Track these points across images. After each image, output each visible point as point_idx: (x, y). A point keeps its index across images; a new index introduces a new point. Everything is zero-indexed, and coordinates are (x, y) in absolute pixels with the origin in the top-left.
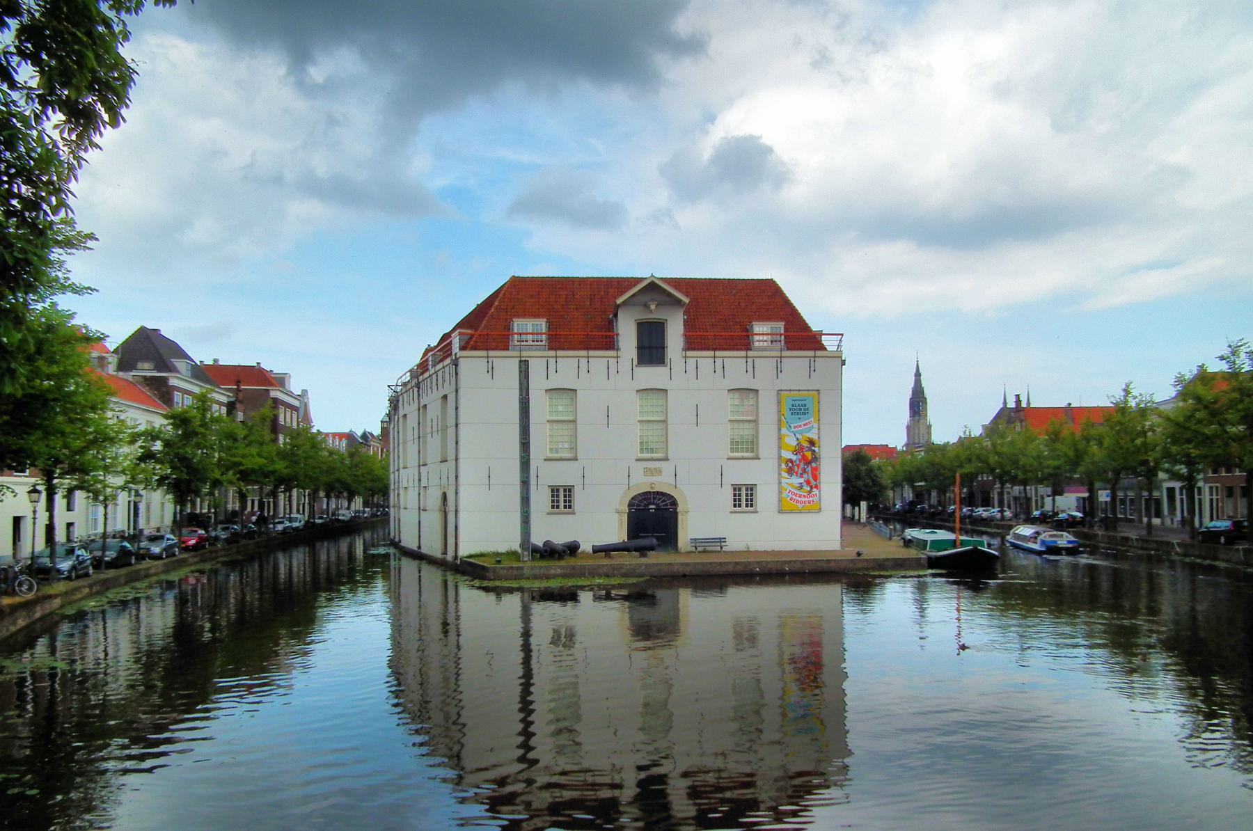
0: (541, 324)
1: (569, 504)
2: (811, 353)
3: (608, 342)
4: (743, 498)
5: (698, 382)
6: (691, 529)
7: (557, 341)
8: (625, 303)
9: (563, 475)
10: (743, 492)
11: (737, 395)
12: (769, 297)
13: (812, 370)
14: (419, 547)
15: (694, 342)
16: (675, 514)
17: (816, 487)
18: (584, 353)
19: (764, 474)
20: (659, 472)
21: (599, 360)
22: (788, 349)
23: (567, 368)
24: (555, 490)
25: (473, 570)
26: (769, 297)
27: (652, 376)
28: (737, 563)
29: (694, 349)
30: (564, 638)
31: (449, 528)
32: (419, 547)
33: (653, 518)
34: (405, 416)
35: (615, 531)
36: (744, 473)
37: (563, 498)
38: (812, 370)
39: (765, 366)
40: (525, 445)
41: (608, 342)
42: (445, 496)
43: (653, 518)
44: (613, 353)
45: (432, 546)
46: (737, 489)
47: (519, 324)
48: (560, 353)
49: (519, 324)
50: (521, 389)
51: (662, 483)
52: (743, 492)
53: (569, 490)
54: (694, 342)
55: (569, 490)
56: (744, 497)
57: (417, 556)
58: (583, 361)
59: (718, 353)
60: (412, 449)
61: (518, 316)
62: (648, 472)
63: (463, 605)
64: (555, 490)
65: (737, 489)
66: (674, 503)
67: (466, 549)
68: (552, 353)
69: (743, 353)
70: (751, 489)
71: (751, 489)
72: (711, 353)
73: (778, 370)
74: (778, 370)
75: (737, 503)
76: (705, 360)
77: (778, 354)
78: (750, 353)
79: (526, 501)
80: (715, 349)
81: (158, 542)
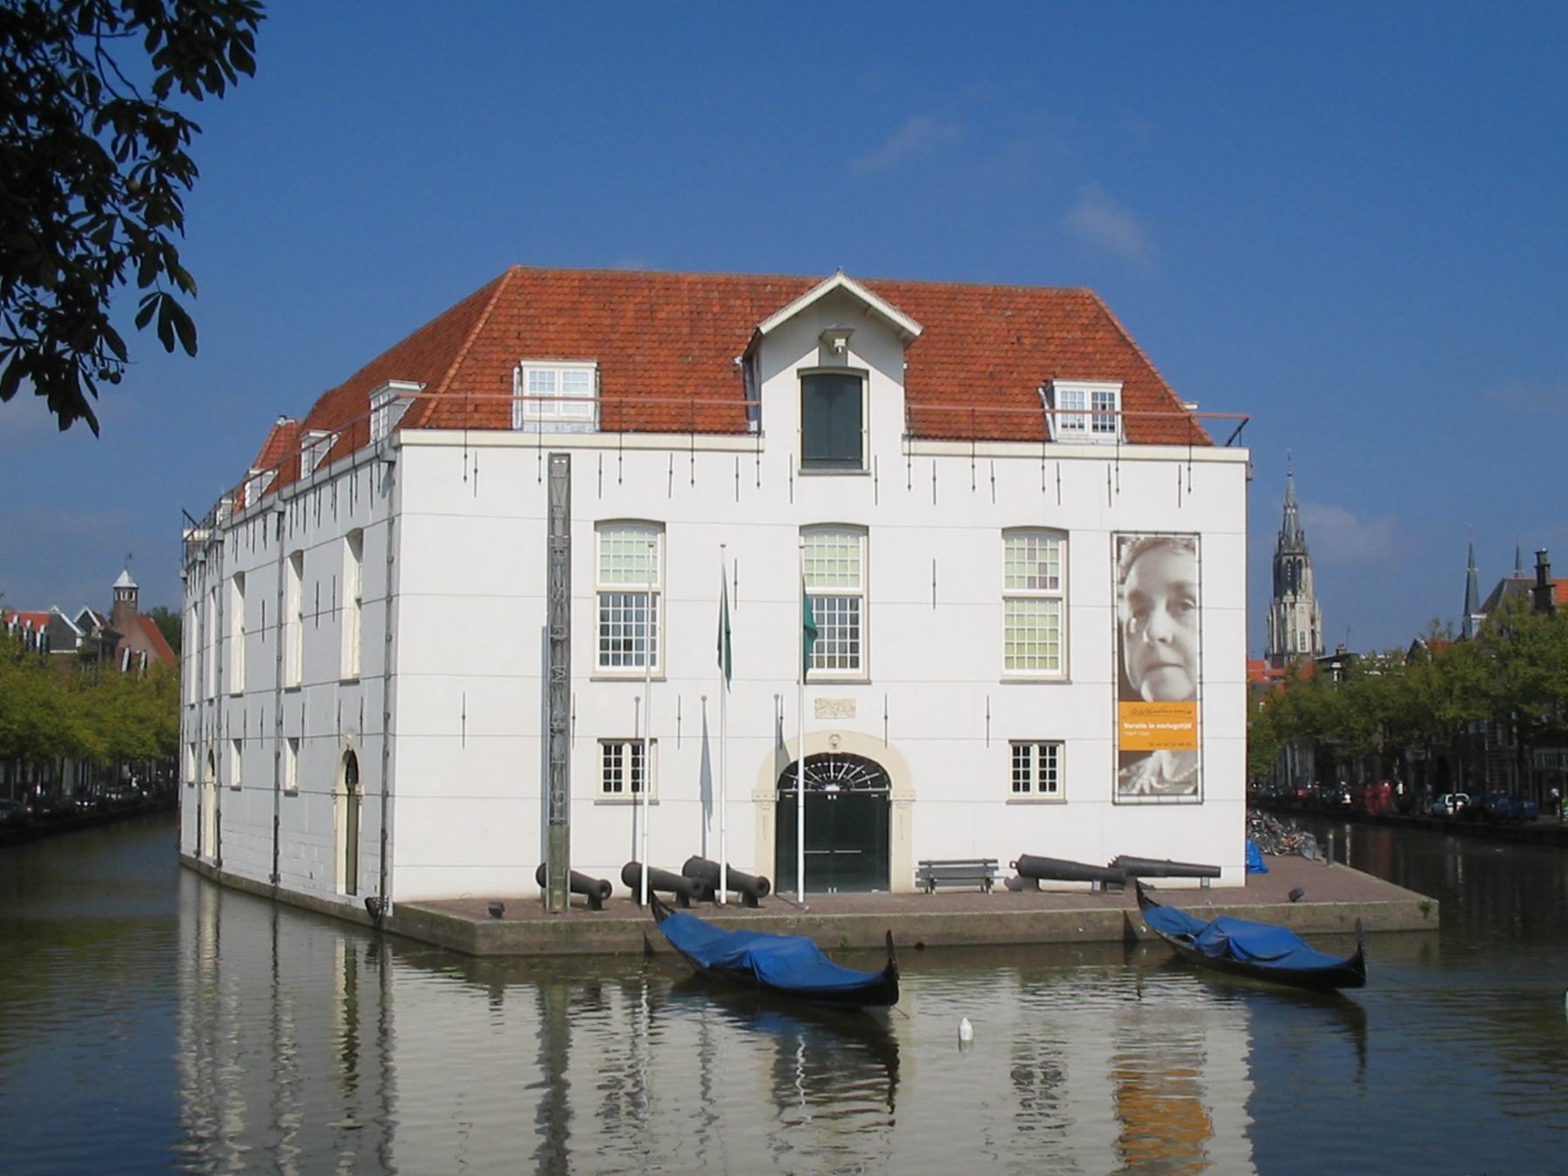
1: (1049, 781)
2: (1182, 452)
3: (740, 419)
4: (1035, 769)
6: (916, 841)
12: (1084, 328)
13: (1183, 488)
14: (275, 878)
15: (921, 427)
16: (887, 805)
17: (561, 732)
19: (1086, 723)
20: (849, 709)
22: (1131, 443)
24: (612, 748)
25: (442, 941)
26: (1084, 328)
27: (832, 494)
28: (1036, 917)
29: (926, 437)
30: (625, 1099)
31: (367, 837)
32: (275, 878)
33: (839, 814)
34: (240, 578)
37: (623, 762)
38: (1183, 488)
41: (740, 419)
42: (351, 761)
45: (318, 872)
46: (1020, 750)
49: (535, 374)
50: (552, 521)
54: (921, 427)
56: (1036, 764)
57: (275, 901)
59: (981, 447)
63: (401, 1023)
64: (612, 748)
66: (882, 779)
67: (414, 883)
68: (612, 439)
70: (1049, 749)
71: (1049, 749)
73: (1112, 488)
74: (1112, 488)
75: (1020, 781)
76: (953, 463)
77: (1112, 452)
78: (1050, 449)
79: (556, 769)
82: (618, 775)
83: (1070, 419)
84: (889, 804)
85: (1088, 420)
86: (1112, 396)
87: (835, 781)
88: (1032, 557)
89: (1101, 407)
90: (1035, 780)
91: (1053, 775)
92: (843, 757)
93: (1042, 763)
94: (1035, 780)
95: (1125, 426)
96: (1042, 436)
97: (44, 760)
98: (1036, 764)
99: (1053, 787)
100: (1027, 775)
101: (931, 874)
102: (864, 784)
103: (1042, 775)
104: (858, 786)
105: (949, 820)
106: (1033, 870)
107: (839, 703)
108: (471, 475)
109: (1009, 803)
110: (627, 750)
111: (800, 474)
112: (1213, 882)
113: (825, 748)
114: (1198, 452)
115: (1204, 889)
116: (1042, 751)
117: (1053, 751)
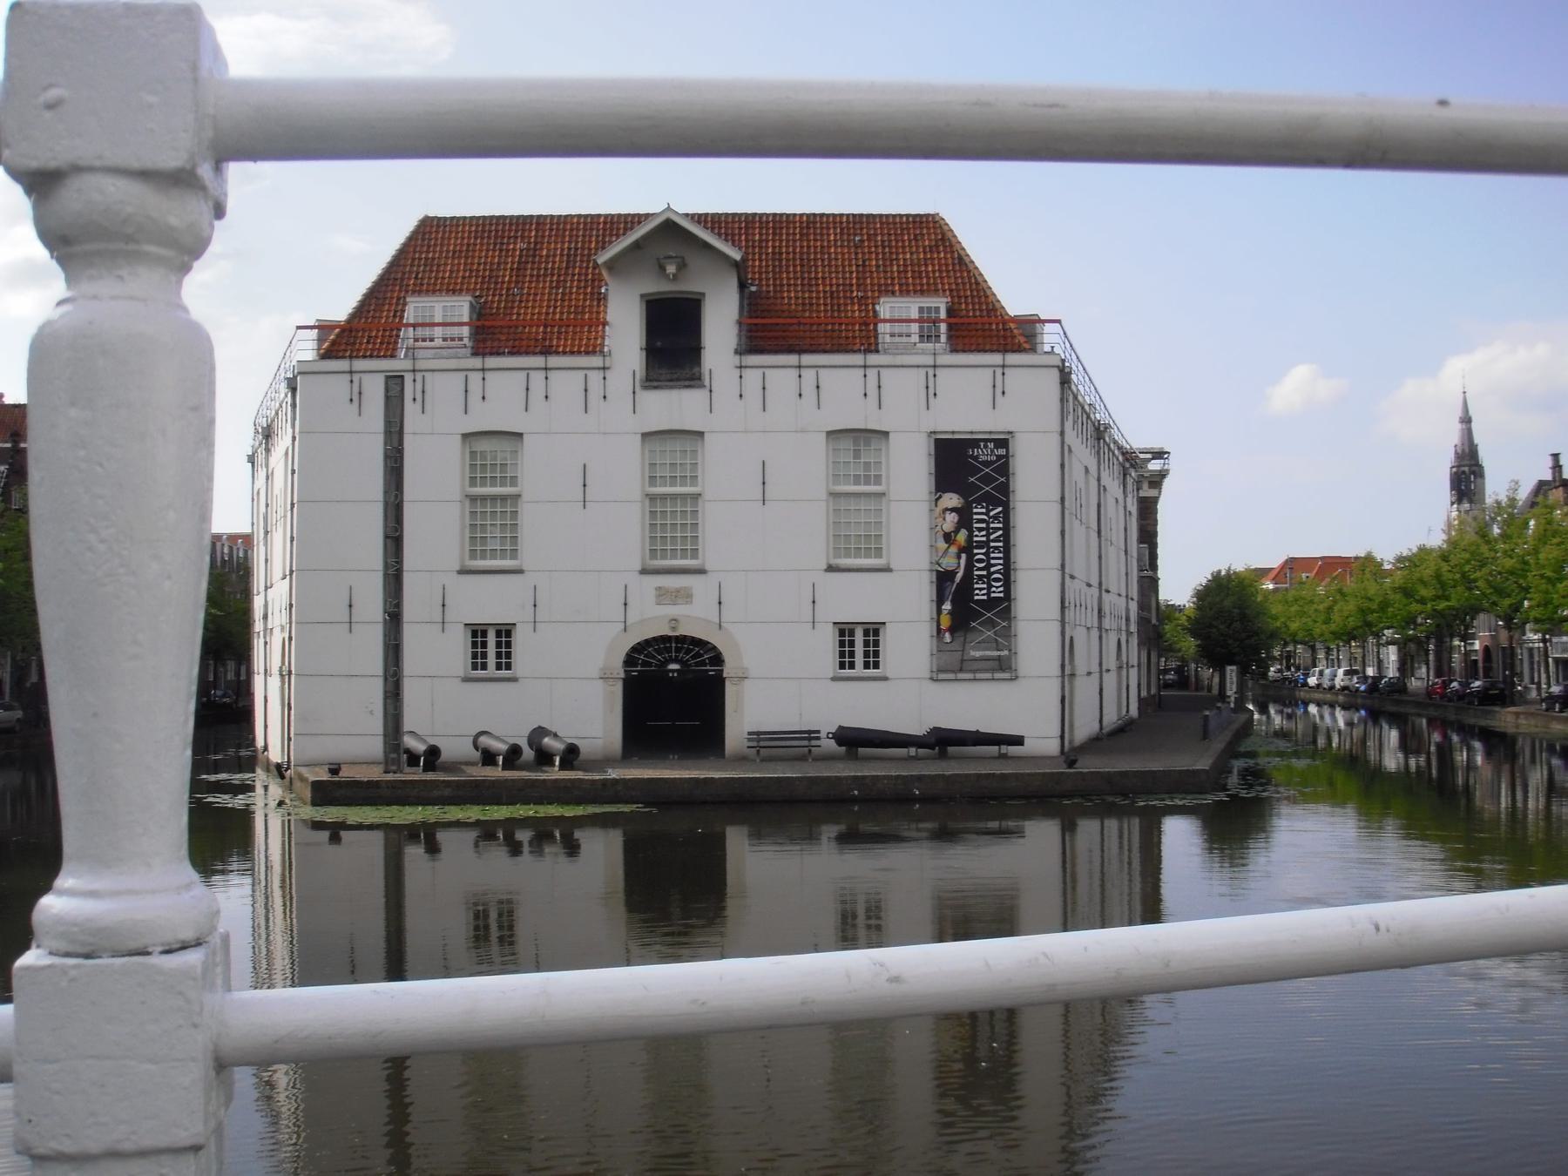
0: (460, 307)
1: (505, 659)
2: (996, 358)
4: (859, 649)
5: (764, 418)
6: (750, 710)
7: (493, 336)
8: (611, 265)
9: (489, 601)
10: (859, 638)
11: (847, 443)
13: (997, 392)
18: (538, 361)
19: (905, 605)
20: (685, 596)
21: (565, 379)
22: (954, 350)
23: (506, 392)
27: (674, 407)
29: (761, 351)
33: (673, 689)
35: (591, 717)
36: (856, 599)
38: (997, 392)
39: (903, 386)
40: (394, 541)
43: (673, 689)
44: (596, 361)
46: (845, 632)
47: (886, 307)
48: (492, 362)
49: (886, 307)
51: (695, 619)
52: (859, 638)
53: (505, 633)
55: (505, 633)
56: (859, 646)
58: (537, 378)
59: (807, 359)
60: (262, 549)
61: (418, 291)
62: (663, 595)
65: (845, 632)
66: (718, 659)
68: (477, 362)
69: (857, 359)
70: (873, 632)
71: (873, 632)
72: (792, 359)
73: (930, 393)
74: (930, 393)
76: (781, 375)
77: (929, 360)
78: (873, 359)
80: (800, 351)
81: (1451, 749)
82: (852, 654)
83: (898, 328)
84: (723, 680)
85: (915, 327)
86: (937, 309)
87: (676, 661)
88: (857, 454)
89: (927, 321)
90: (859, 659)
91: (509, 655)
92: (682, 639)
93: (866, 644)
94: (859, 659)
95: (949, 338)
96: (870, 345)
97: (1211, 626)
98: (859, 646)
99: (876, 665)
100: (484, 655)
101: (766, 743)
102: (703, 663)
103: (866, 654)
104: (697, 664)
105: (780, 692)
106: (852, 740)
107: (678, 591)
108: (356, 398)
109: (834, 679)
110: (491, 639)
111: (645, 388)
112: (1013, 750)
113: (665, 631)
114: (1012, 358)
115: (1003, 756)
116: (866, 633)
117: (876, 632)
